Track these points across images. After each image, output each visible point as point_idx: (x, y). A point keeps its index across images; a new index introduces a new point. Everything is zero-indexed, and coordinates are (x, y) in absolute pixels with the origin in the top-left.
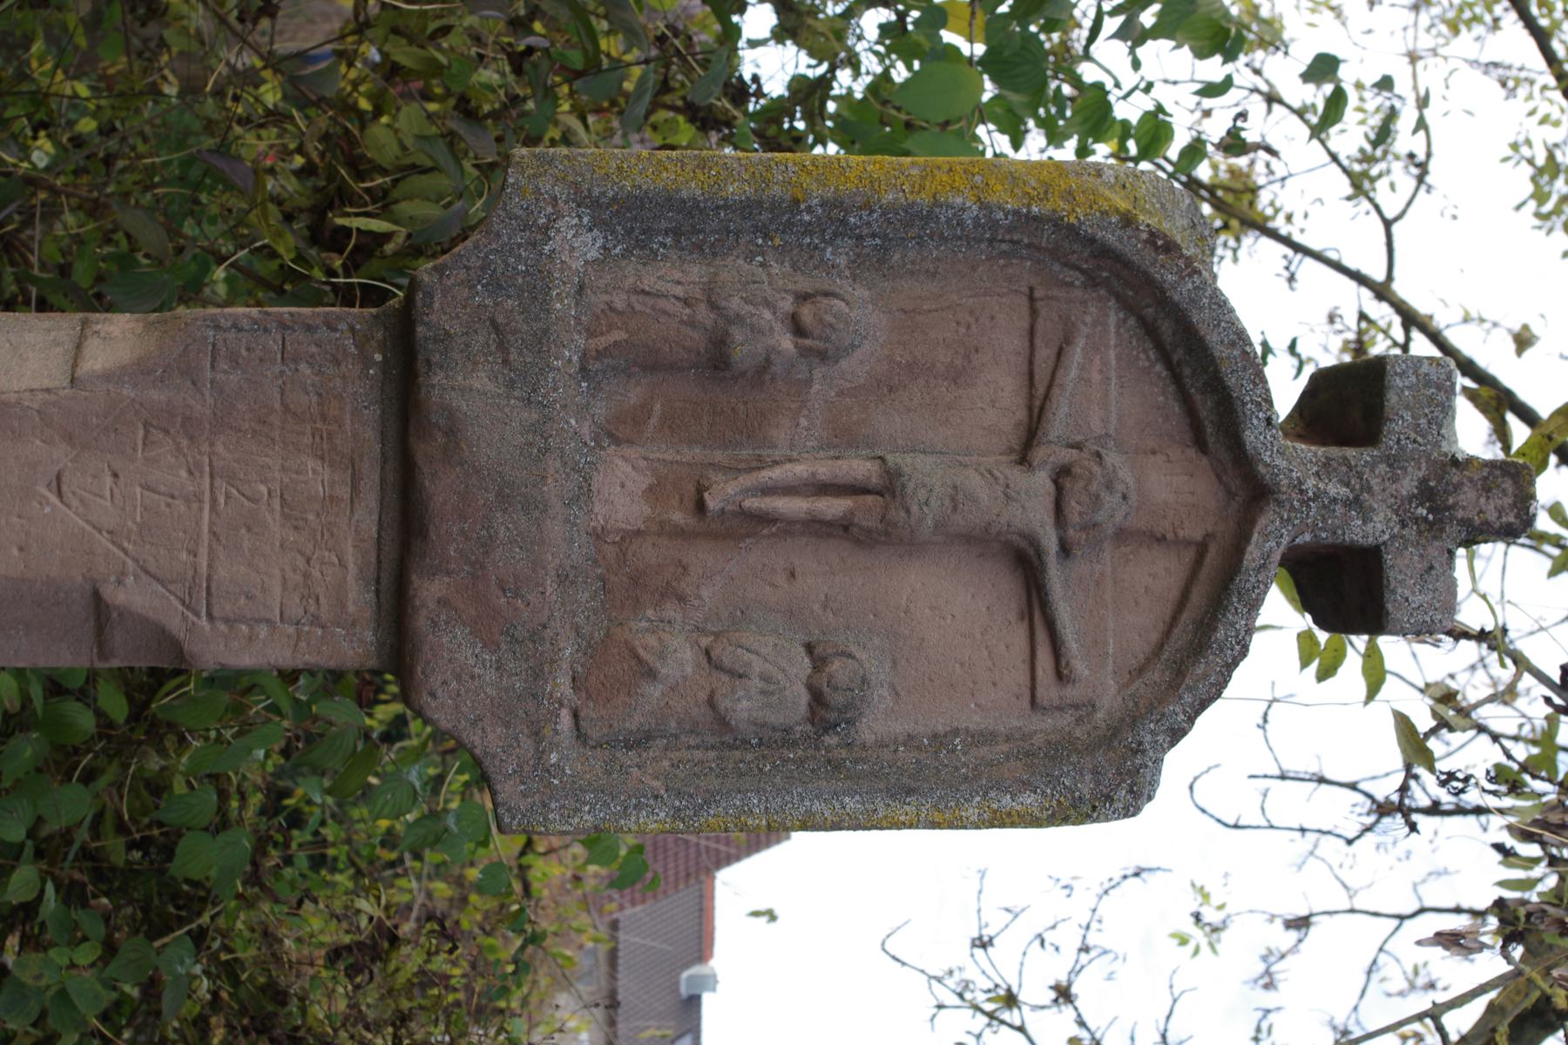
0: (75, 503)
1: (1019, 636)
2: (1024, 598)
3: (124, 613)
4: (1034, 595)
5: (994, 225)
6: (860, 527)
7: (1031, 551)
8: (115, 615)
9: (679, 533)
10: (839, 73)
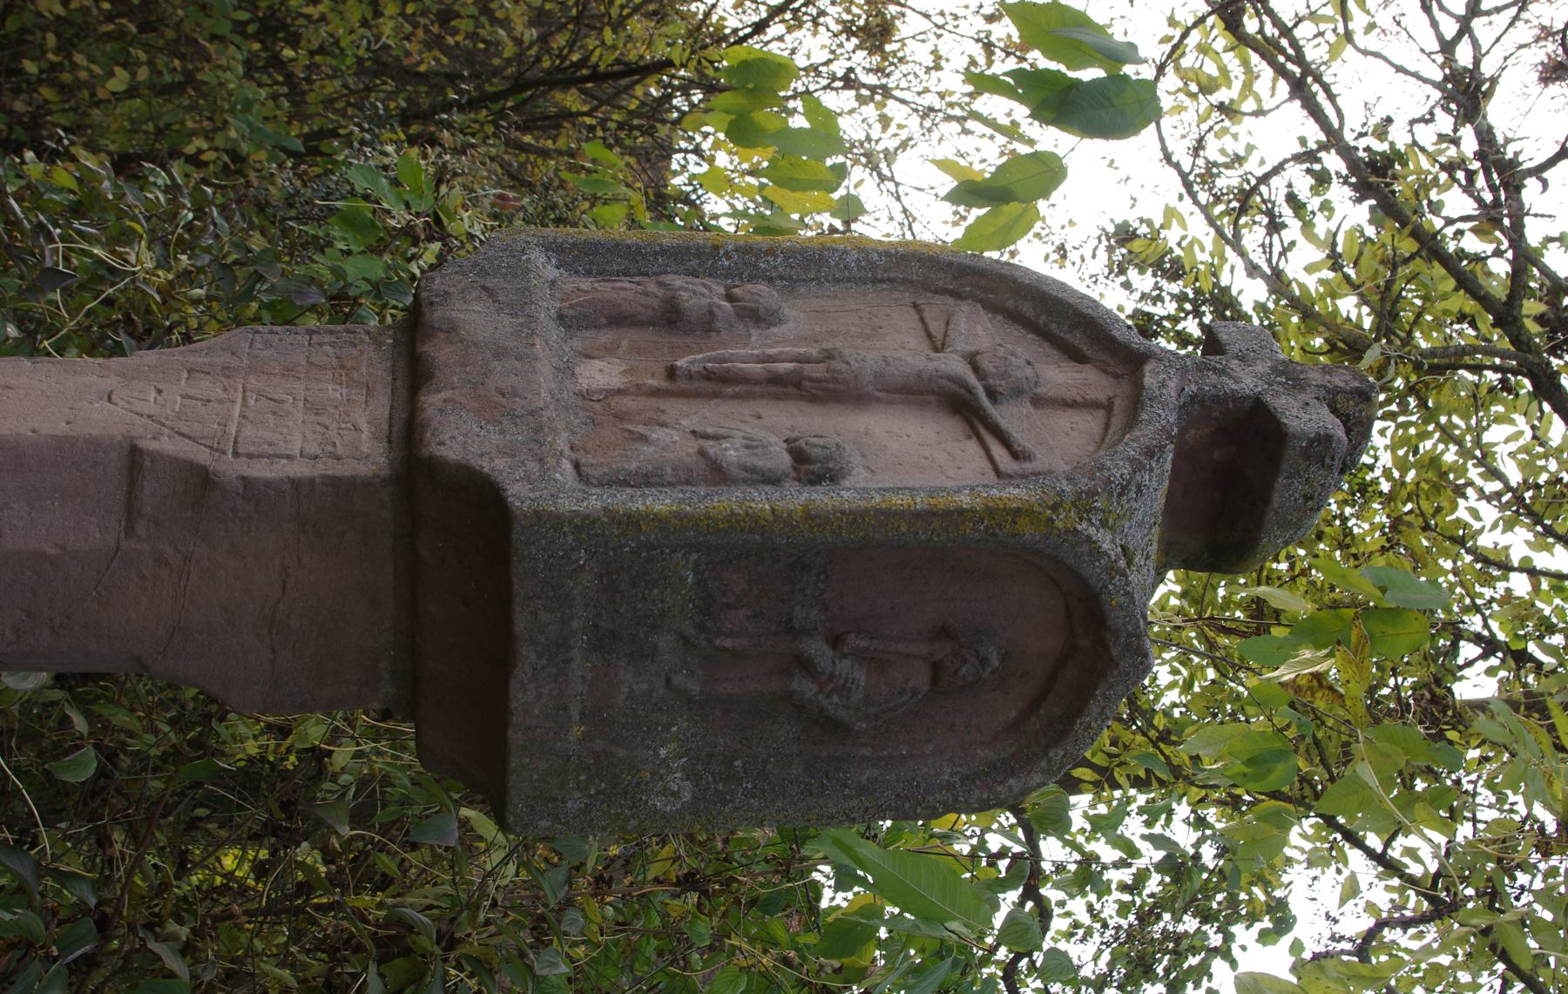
0: (121, 403)
1: (972, 447)
2: (967, 428)
3: (156, 457)
4: (982, 431)
5: (873, 266)
6: (811, 380)
7: (962, 391)
8: (147, 463)
9: (656, 393)
10: (1043, 845)
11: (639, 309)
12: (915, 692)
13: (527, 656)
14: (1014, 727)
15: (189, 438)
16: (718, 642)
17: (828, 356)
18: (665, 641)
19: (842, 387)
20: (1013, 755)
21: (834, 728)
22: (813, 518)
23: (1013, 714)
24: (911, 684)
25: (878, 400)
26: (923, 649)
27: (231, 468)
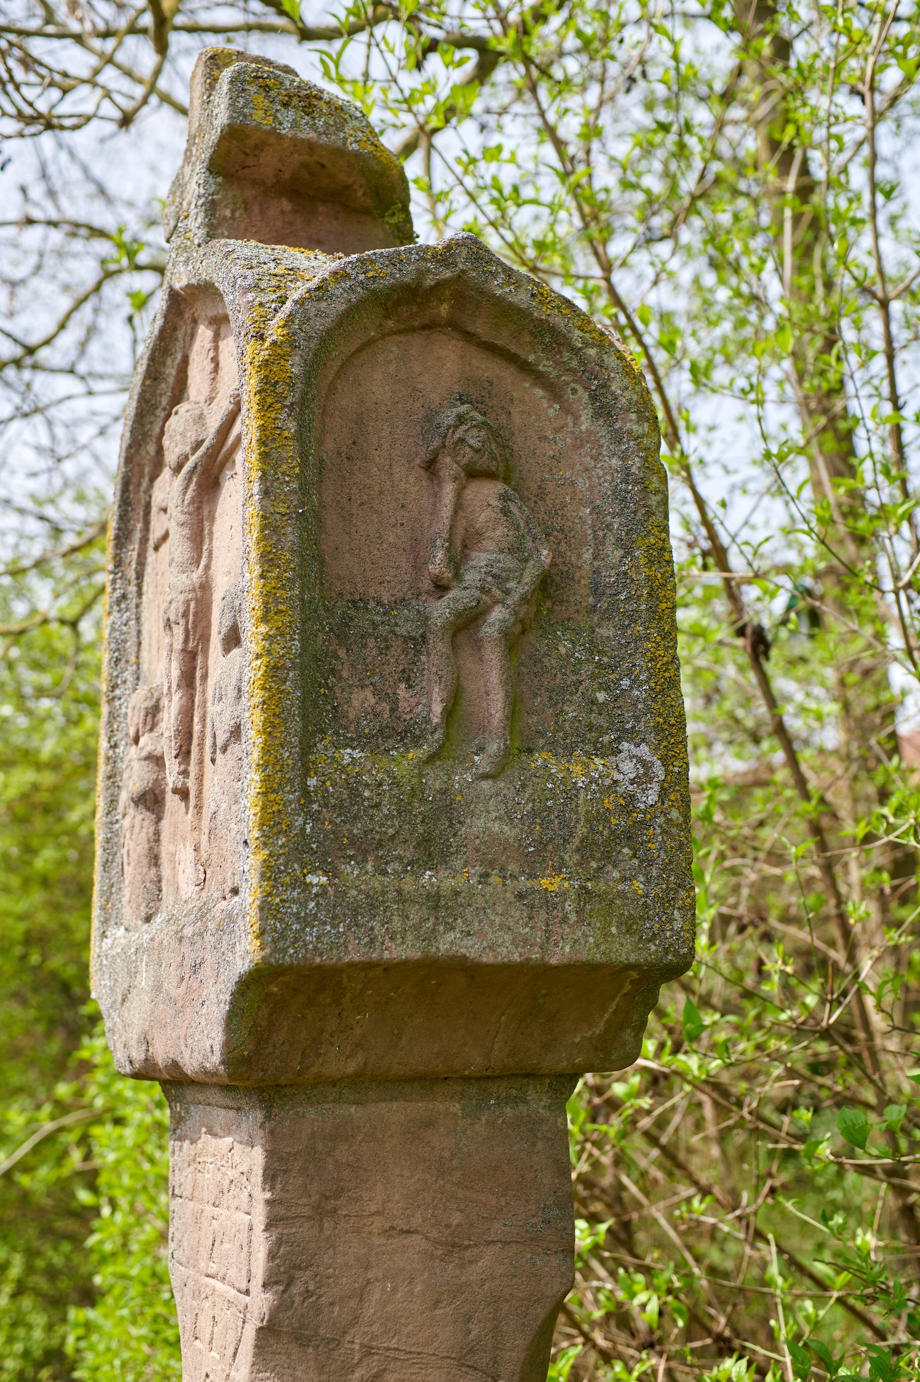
4: (225, 449)
11: (143, 834)
12: (504, 497)
13: (448, 943)
14: (554, 391)
15: (238, 1345)
16: (436, 720)
17: (168, 625)
18: (434, 781)
19: (192, 605)
20: (586, 388)
21: (549, 585)
22: (267, 610)
23: (539, 392)
24: (495, 502)
25: (208, 567)
26: (449, 490)
27: (261, 1302)
